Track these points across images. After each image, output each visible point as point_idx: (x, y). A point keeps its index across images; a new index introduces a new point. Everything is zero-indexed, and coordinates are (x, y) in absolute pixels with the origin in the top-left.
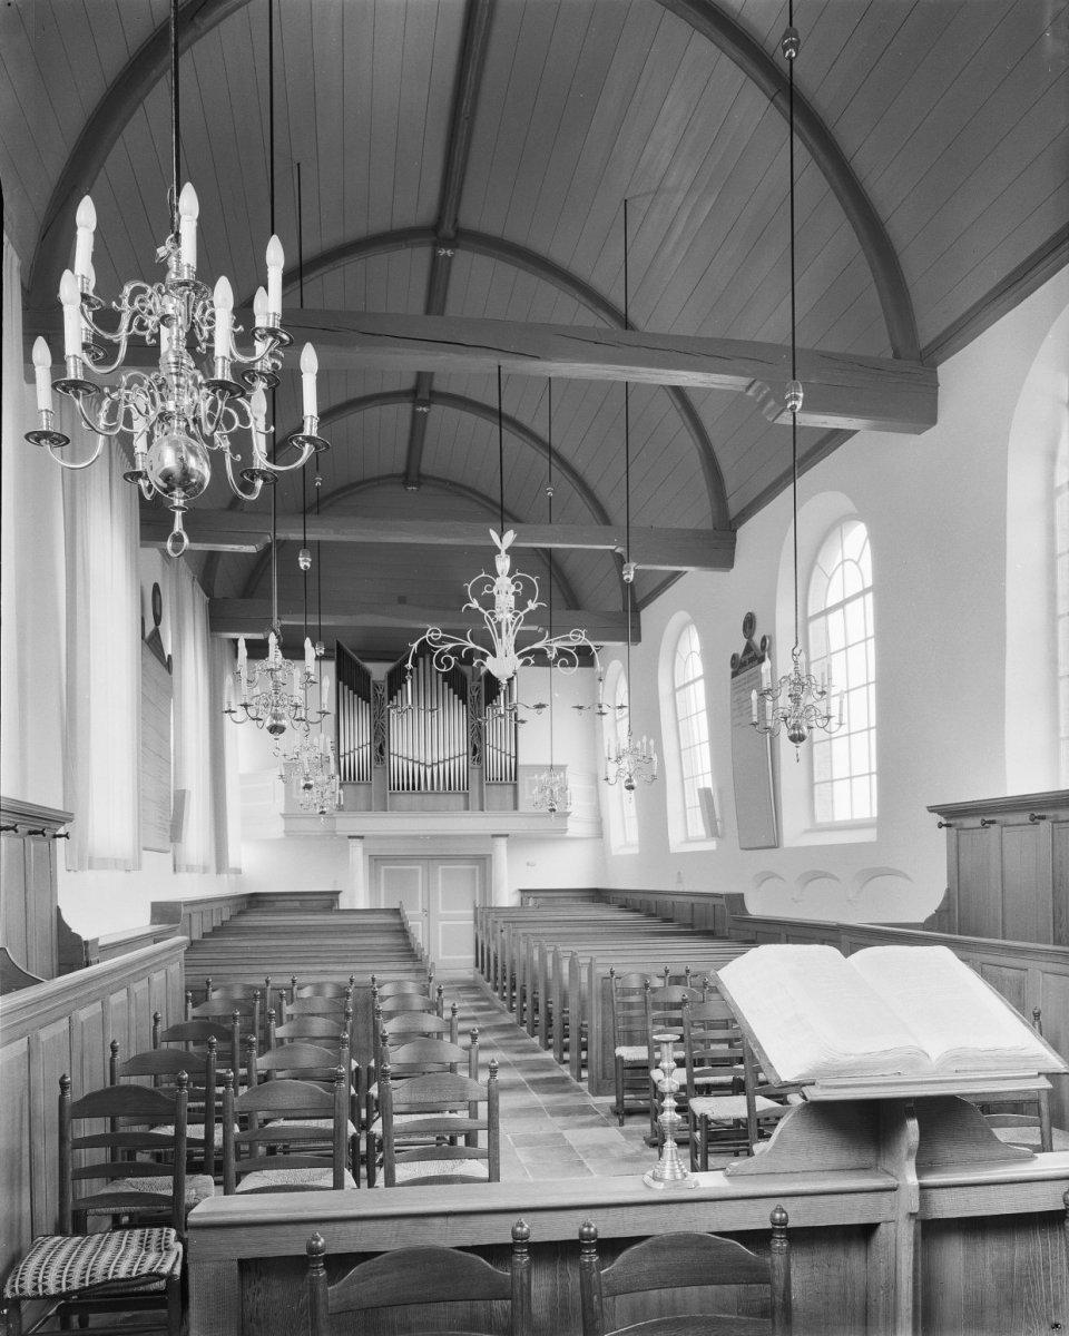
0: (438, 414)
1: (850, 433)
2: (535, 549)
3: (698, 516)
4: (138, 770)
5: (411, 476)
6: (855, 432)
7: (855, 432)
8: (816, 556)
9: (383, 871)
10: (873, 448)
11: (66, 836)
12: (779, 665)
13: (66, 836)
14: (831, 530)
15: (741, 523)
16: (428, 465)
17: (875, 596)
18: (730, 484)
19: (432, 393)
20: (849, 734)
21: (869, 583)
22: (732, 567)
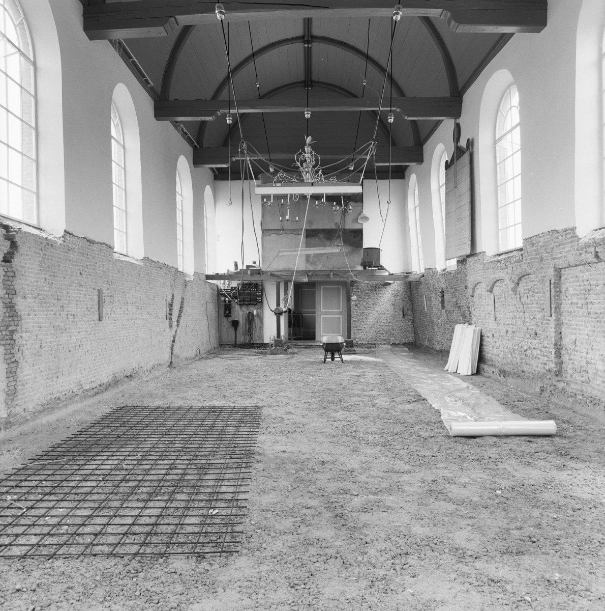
0: (316, 46)
1: (512, 34)
2: (367, 111)
3: (444, 91)
4: (23, 140)
5: (308, 82)
6: (513, 34)
7: (513, 34)
8: (499, 107)
9: (322, 287)
10: (521, 41)
11: (325, 362)
12: (507, 368)
13: (325, 362)
14: (503, 95)
15: (464, 92)
16: (315, 77)
17: (521, 128)
18: (458, 73)
19: (312, 37)
20: (515, 225)
21: (520, 172)
22: (460, 116)
